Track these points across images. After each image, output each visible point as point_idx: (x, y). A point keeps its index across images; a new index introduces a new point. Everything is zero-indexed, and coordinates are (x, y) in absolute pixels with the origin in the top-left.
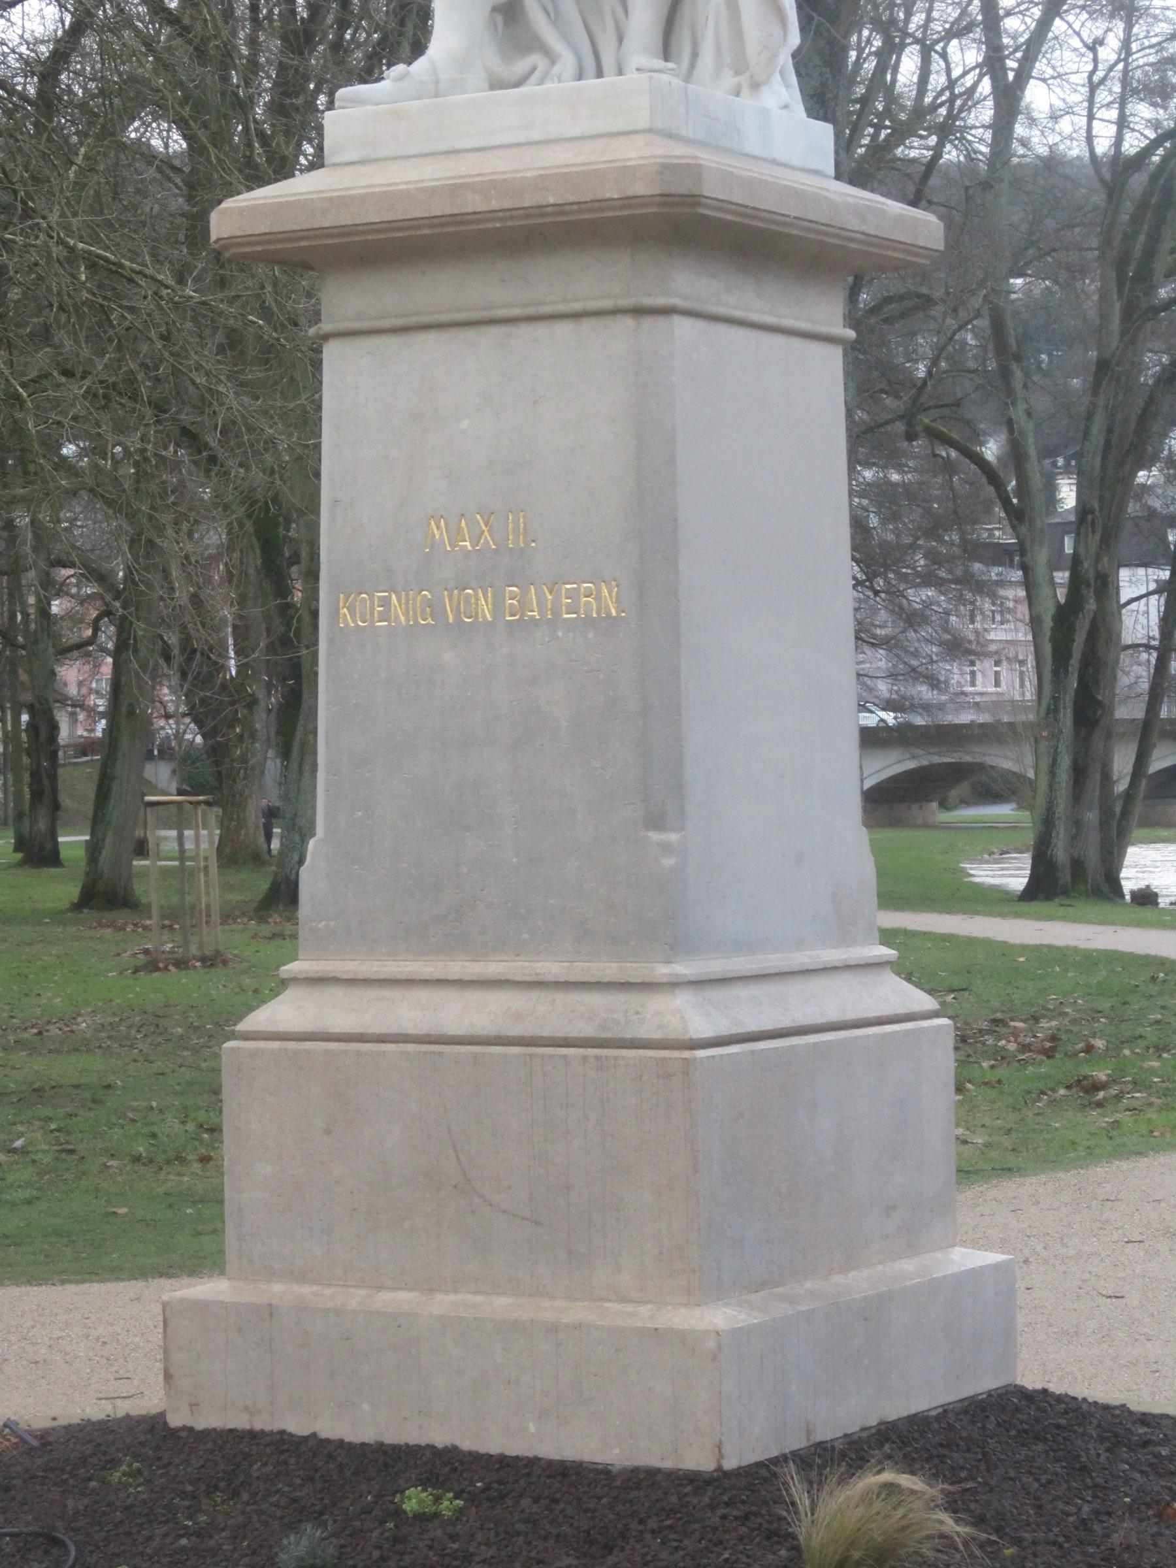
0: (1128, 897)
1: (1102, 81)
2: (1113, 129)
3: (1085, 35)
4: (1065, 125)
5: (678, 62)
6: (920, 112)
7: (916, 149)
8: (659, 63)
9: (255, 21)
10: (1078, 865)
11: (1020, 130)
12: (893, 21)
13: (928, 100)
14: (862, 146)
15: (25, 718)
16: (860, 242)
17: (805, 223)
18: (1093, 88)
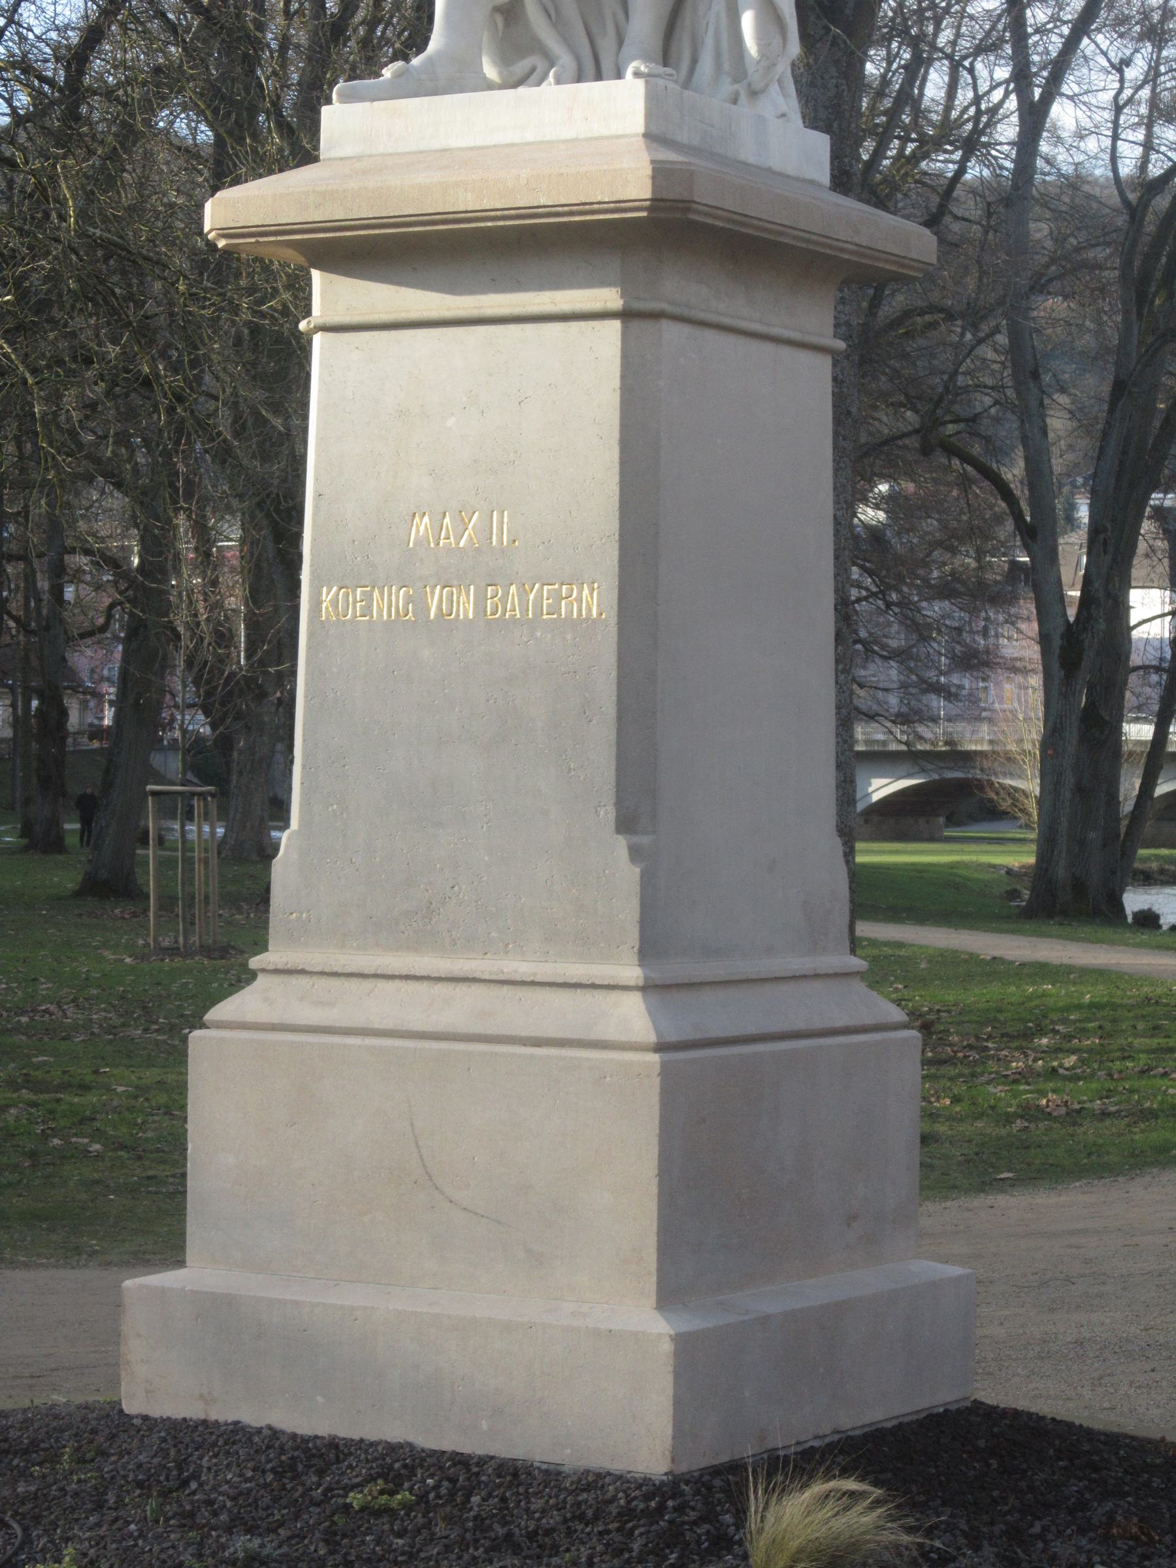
0: (1130, 919)
1: (1130, 100)
2: (1139, 151)
3: (1112, 55)
4: (1091, 144)
5: (677, 68)
6: (947, 127)
7: (942, 164)
8: (661, 70)
10: (1079, 887)
11: (1044, 147)
12: (922, 36)
13: (954, 114)
14: (891, 157)
15: (35, 703)
16: (852, 253)
17: (796, 232)
18: (1118, 109)
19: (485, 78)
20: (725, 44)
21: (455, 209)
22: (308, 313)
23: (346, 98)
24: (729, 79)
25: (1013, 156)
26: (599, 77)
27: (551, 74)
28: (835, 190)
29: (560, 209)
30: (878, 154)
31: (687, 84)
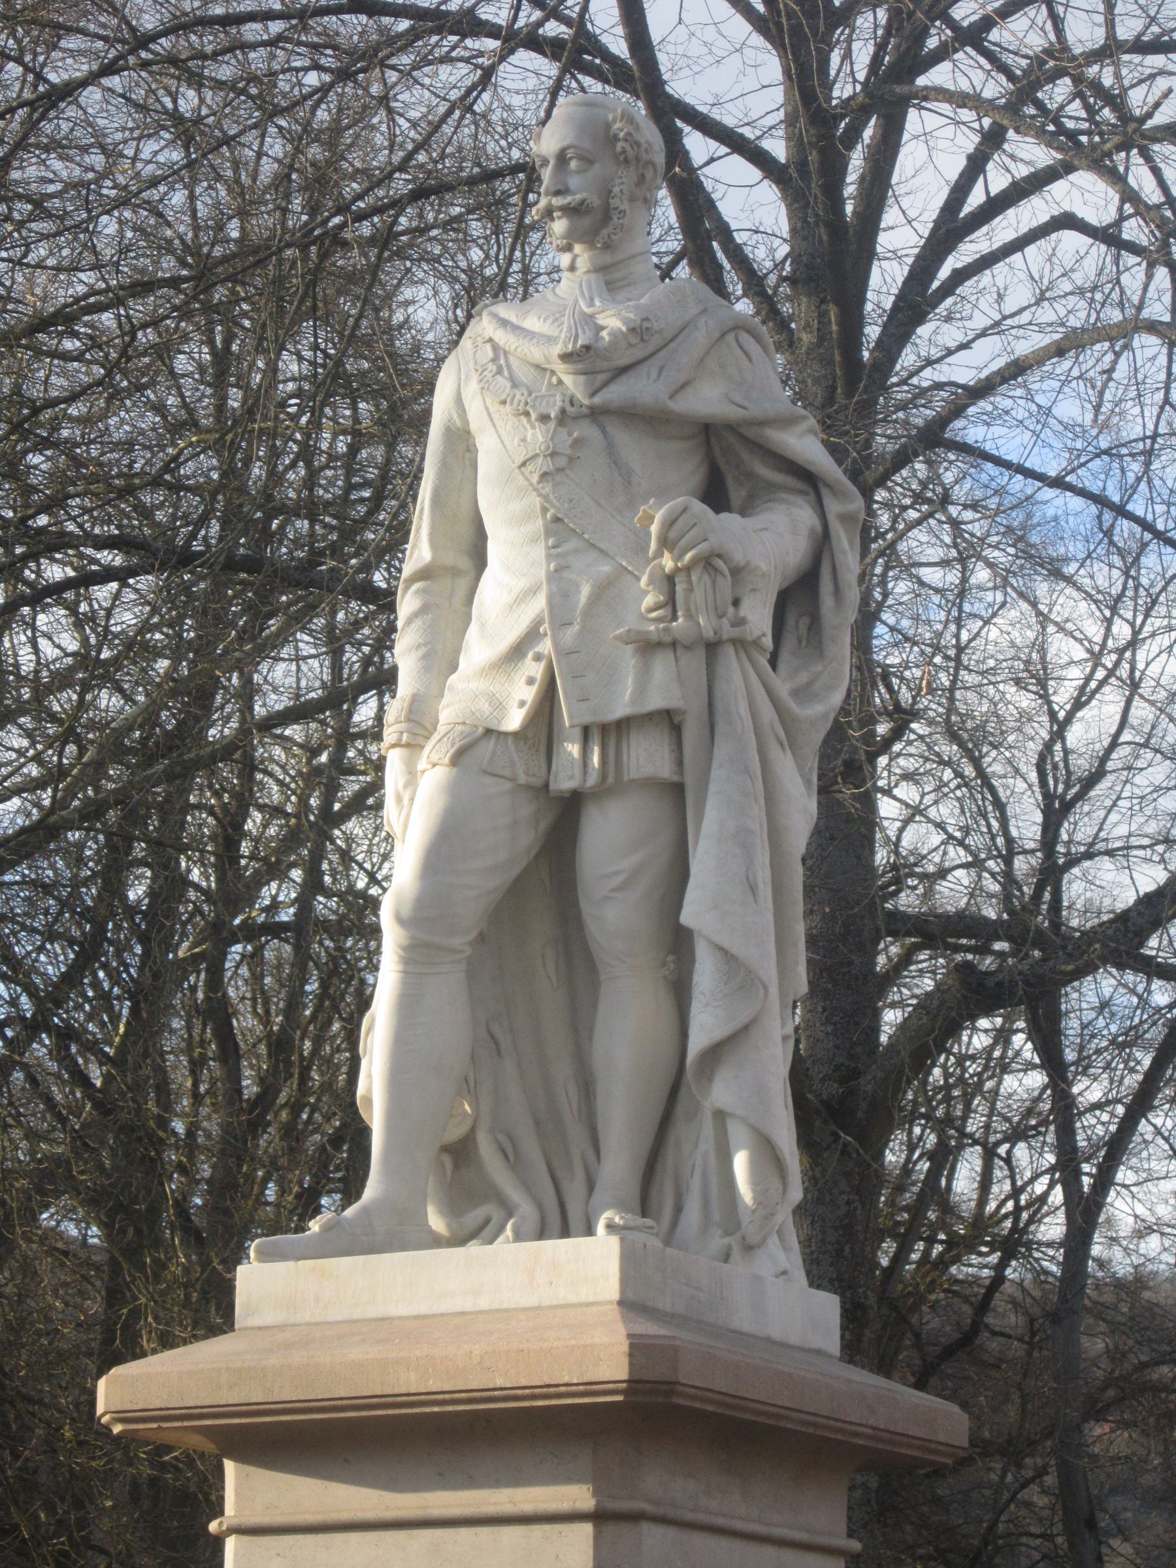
5: (657, 1220)
7: (977, 1266)
8: (640, 1221)
9: (197, 1098)
11: (1096, 1250)
12: (948, 1120)
13: (991, 1206)
16: (868, 1437)
19: (430, 1231)
20: (714, 1188)
21: (396, 1391)
22: (217, 1510)
23: (266, 1256)
24: (720, 1231)
25: (1061, 1259)
26: (565, 1233)
27: (509, 1226)
28: (850, 1362)
29: (520, 1392)
30: (899, 1258)
31: (668, 1240)
